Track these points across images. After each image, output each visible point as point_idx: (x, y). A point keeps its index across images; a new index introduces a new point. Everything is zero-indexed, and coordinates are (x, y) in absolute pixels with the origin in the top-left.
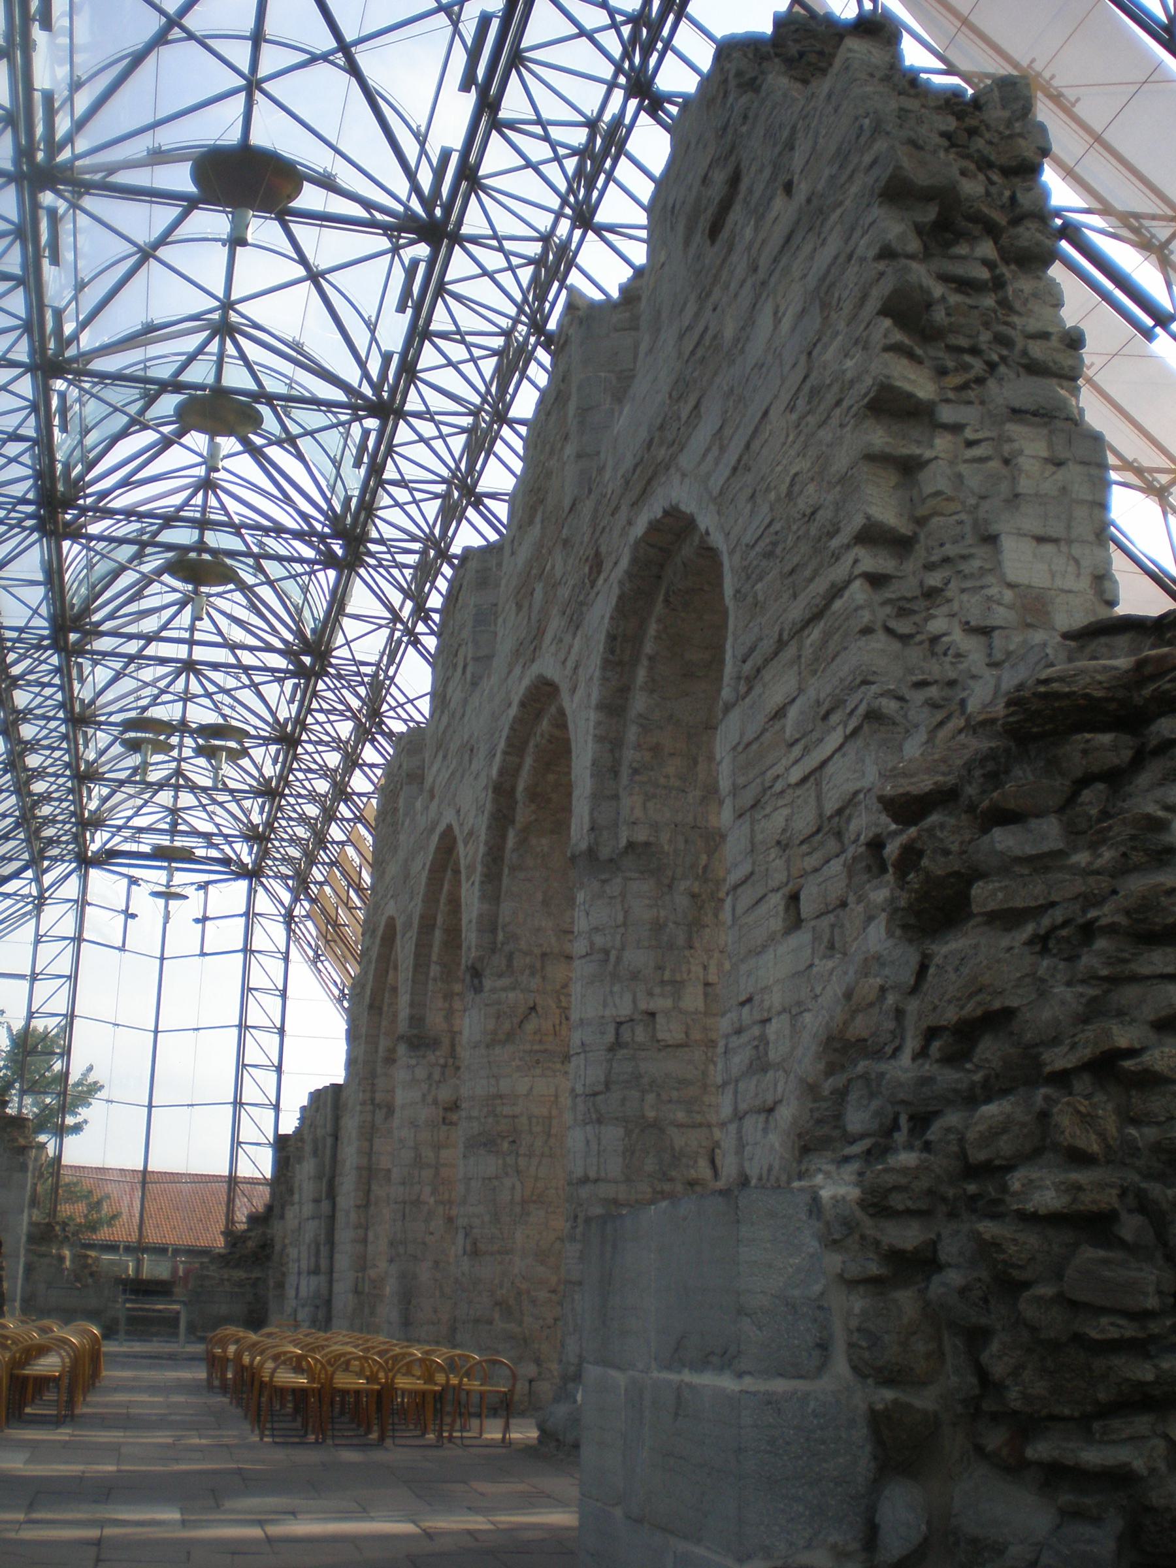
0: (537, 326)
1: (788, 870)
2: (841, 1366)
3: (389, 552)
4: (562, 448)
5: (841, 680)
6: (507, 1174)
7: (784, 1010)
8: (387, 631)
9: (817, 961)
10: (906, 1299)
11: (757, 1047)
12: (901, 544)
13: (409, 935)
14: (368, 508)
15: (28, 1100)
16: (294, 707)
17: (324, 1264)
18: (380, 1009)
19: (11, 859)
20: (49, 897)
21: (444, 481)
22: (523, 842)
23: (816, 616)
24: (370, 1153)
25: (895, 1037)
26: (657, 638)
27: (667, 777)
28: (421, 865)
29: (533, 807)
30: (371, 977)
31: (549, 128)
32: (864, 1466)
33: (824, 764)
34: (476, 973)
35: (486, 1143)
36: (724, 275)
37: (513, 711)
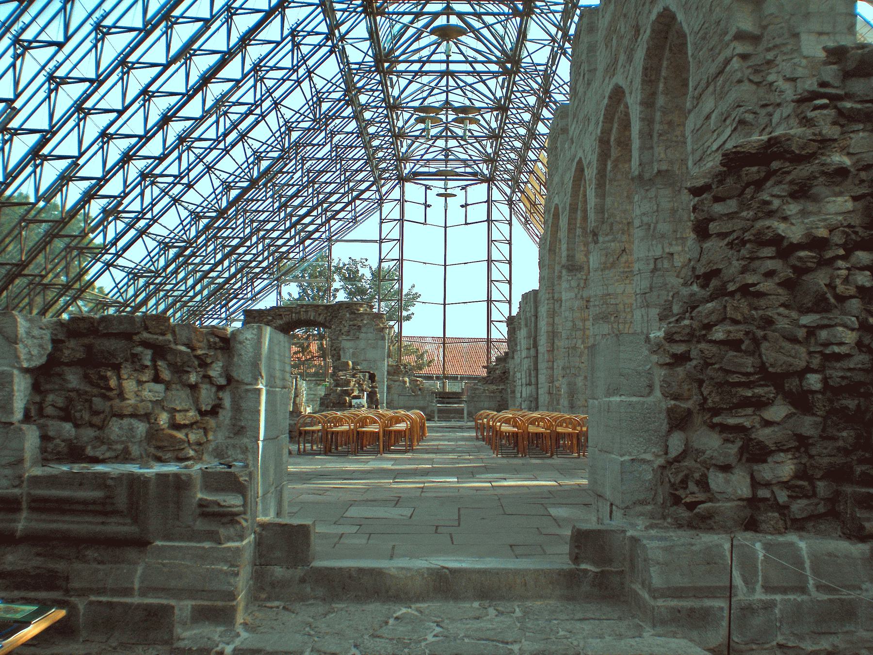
2: (658, 393)
3: (546, 5)
10: (680, 371)
12: (755, 39)
15: (383, 304)
17: (533, 380)
18: (555, 251)
19: (364, 181)
22: (615, 166)
23: (721, 72)
24: (553, 324)
26: (667, 68)
27: (676, 136)
28: (569, 177)
32: (665, 427)
34: (595, 234)
35: (603, 318)
37: (606, 101)
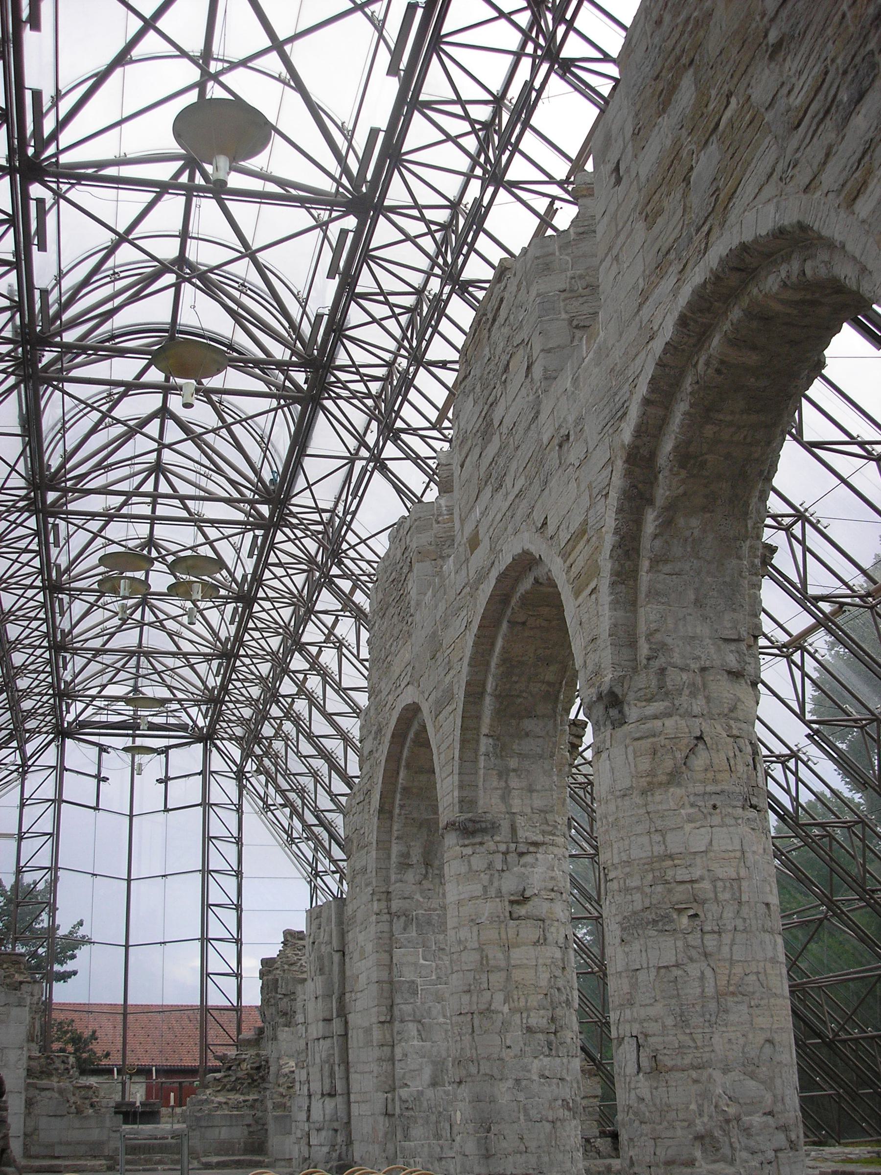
6: (691, 960)
16: (219, 679)
17: (340, 1087)
18: (391, 812)
20: (32, 765)
22: (667, 524)
24: (390, 966)
29: (683, 474)
31: (424, 211)
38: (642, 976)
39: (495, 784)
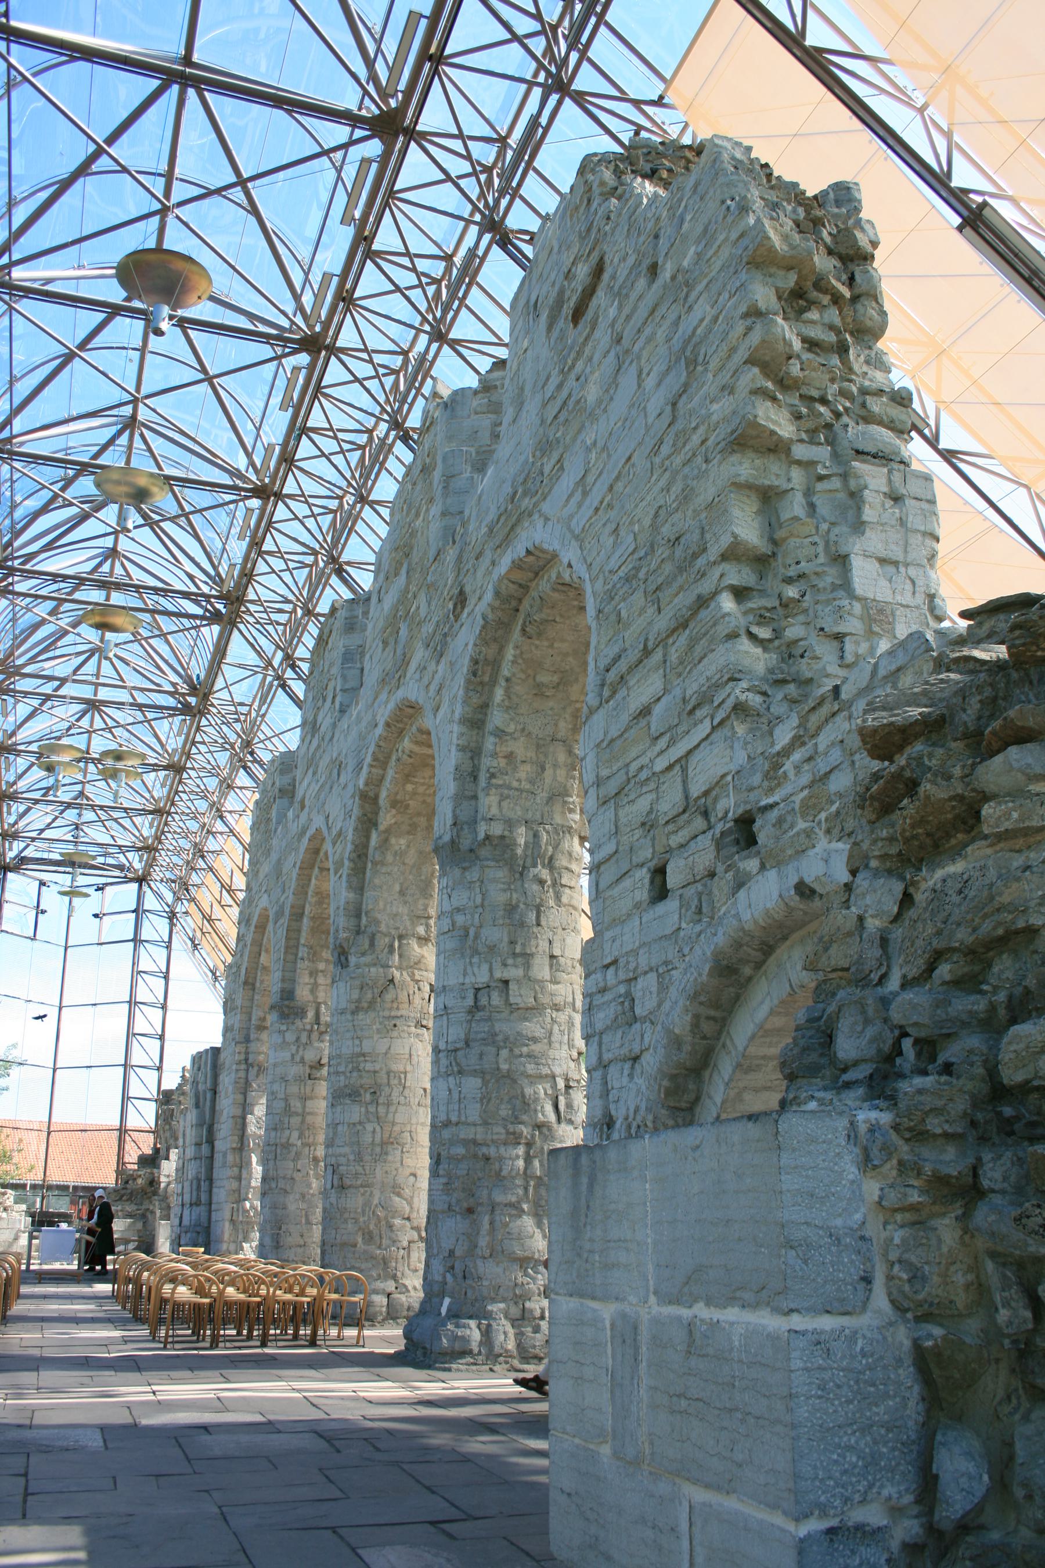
0: (396, 424)
1: (653, 846)
2: (880, 1300)
3: (265, 612)
4: (427, 510)
5: (708, 679)
7: (651, 969)
8: (260, 676)
9: (684, 925)
11: (623, 1003)
13: (281, 921)
14: (248, 576)
17: (204, 1197)
18: (253, 985)
21: (315, 553)
25: (881, 965)
27: (519, 780)
29: (394, 811)
30: (246, 958)
32: (914, 1410)
33: (690, 752)
36: (587, 350)
37: (379, 730)
38: (340, 1128)
39: (307, 980)
